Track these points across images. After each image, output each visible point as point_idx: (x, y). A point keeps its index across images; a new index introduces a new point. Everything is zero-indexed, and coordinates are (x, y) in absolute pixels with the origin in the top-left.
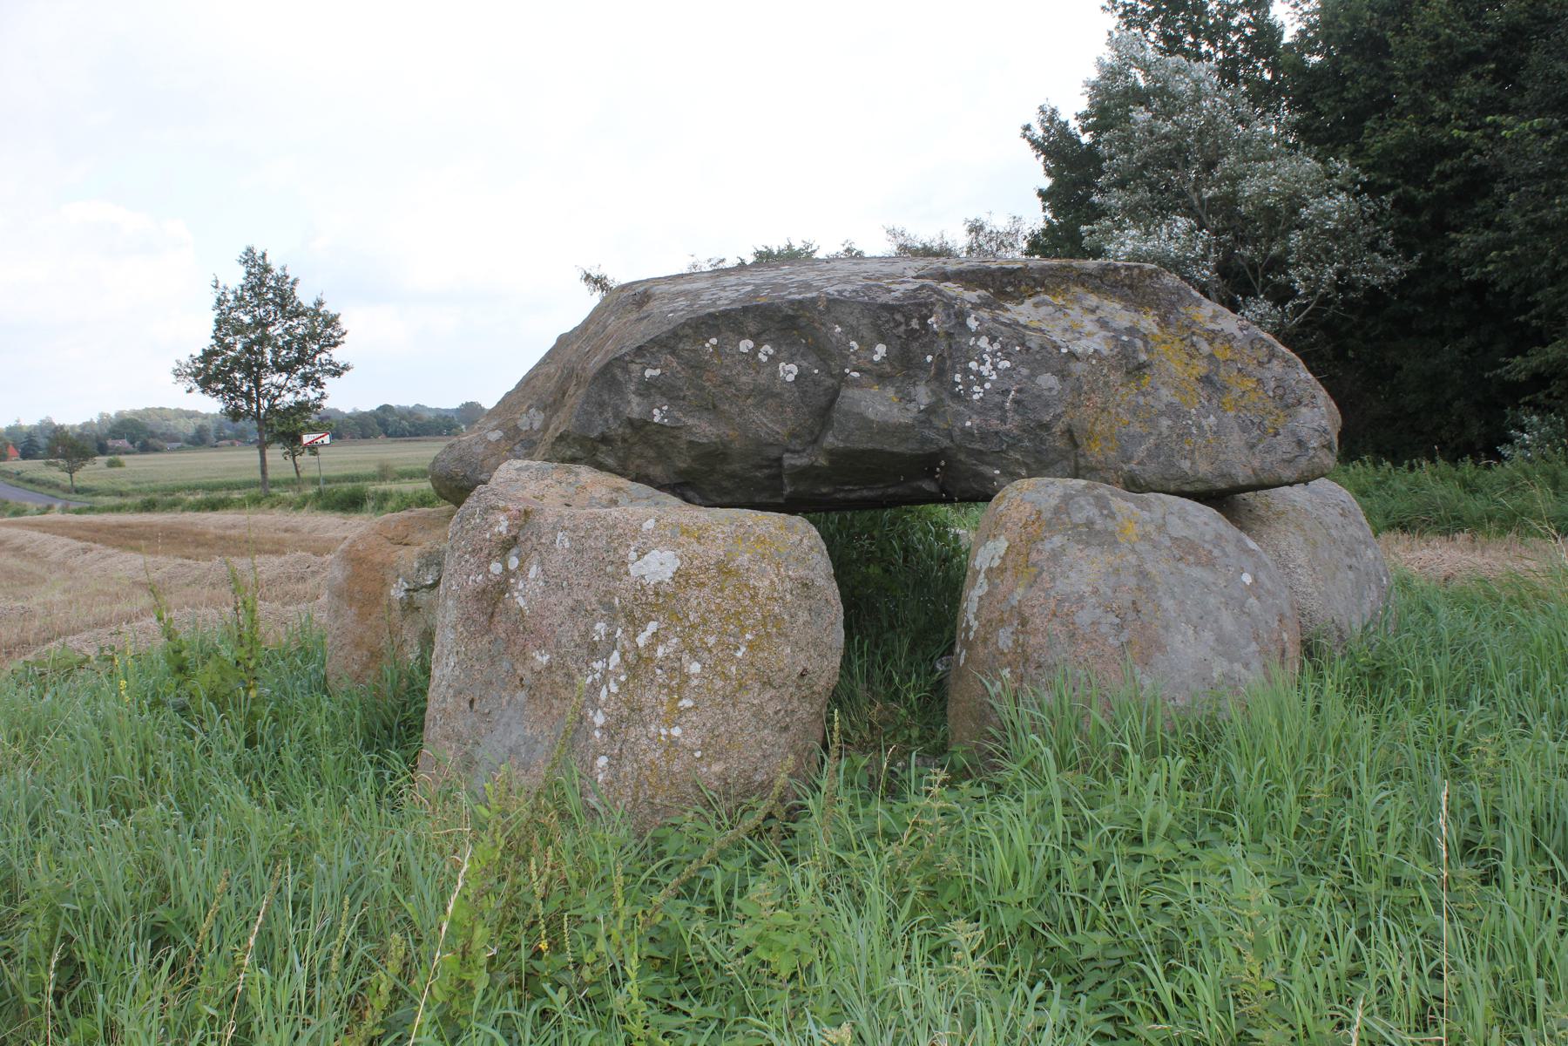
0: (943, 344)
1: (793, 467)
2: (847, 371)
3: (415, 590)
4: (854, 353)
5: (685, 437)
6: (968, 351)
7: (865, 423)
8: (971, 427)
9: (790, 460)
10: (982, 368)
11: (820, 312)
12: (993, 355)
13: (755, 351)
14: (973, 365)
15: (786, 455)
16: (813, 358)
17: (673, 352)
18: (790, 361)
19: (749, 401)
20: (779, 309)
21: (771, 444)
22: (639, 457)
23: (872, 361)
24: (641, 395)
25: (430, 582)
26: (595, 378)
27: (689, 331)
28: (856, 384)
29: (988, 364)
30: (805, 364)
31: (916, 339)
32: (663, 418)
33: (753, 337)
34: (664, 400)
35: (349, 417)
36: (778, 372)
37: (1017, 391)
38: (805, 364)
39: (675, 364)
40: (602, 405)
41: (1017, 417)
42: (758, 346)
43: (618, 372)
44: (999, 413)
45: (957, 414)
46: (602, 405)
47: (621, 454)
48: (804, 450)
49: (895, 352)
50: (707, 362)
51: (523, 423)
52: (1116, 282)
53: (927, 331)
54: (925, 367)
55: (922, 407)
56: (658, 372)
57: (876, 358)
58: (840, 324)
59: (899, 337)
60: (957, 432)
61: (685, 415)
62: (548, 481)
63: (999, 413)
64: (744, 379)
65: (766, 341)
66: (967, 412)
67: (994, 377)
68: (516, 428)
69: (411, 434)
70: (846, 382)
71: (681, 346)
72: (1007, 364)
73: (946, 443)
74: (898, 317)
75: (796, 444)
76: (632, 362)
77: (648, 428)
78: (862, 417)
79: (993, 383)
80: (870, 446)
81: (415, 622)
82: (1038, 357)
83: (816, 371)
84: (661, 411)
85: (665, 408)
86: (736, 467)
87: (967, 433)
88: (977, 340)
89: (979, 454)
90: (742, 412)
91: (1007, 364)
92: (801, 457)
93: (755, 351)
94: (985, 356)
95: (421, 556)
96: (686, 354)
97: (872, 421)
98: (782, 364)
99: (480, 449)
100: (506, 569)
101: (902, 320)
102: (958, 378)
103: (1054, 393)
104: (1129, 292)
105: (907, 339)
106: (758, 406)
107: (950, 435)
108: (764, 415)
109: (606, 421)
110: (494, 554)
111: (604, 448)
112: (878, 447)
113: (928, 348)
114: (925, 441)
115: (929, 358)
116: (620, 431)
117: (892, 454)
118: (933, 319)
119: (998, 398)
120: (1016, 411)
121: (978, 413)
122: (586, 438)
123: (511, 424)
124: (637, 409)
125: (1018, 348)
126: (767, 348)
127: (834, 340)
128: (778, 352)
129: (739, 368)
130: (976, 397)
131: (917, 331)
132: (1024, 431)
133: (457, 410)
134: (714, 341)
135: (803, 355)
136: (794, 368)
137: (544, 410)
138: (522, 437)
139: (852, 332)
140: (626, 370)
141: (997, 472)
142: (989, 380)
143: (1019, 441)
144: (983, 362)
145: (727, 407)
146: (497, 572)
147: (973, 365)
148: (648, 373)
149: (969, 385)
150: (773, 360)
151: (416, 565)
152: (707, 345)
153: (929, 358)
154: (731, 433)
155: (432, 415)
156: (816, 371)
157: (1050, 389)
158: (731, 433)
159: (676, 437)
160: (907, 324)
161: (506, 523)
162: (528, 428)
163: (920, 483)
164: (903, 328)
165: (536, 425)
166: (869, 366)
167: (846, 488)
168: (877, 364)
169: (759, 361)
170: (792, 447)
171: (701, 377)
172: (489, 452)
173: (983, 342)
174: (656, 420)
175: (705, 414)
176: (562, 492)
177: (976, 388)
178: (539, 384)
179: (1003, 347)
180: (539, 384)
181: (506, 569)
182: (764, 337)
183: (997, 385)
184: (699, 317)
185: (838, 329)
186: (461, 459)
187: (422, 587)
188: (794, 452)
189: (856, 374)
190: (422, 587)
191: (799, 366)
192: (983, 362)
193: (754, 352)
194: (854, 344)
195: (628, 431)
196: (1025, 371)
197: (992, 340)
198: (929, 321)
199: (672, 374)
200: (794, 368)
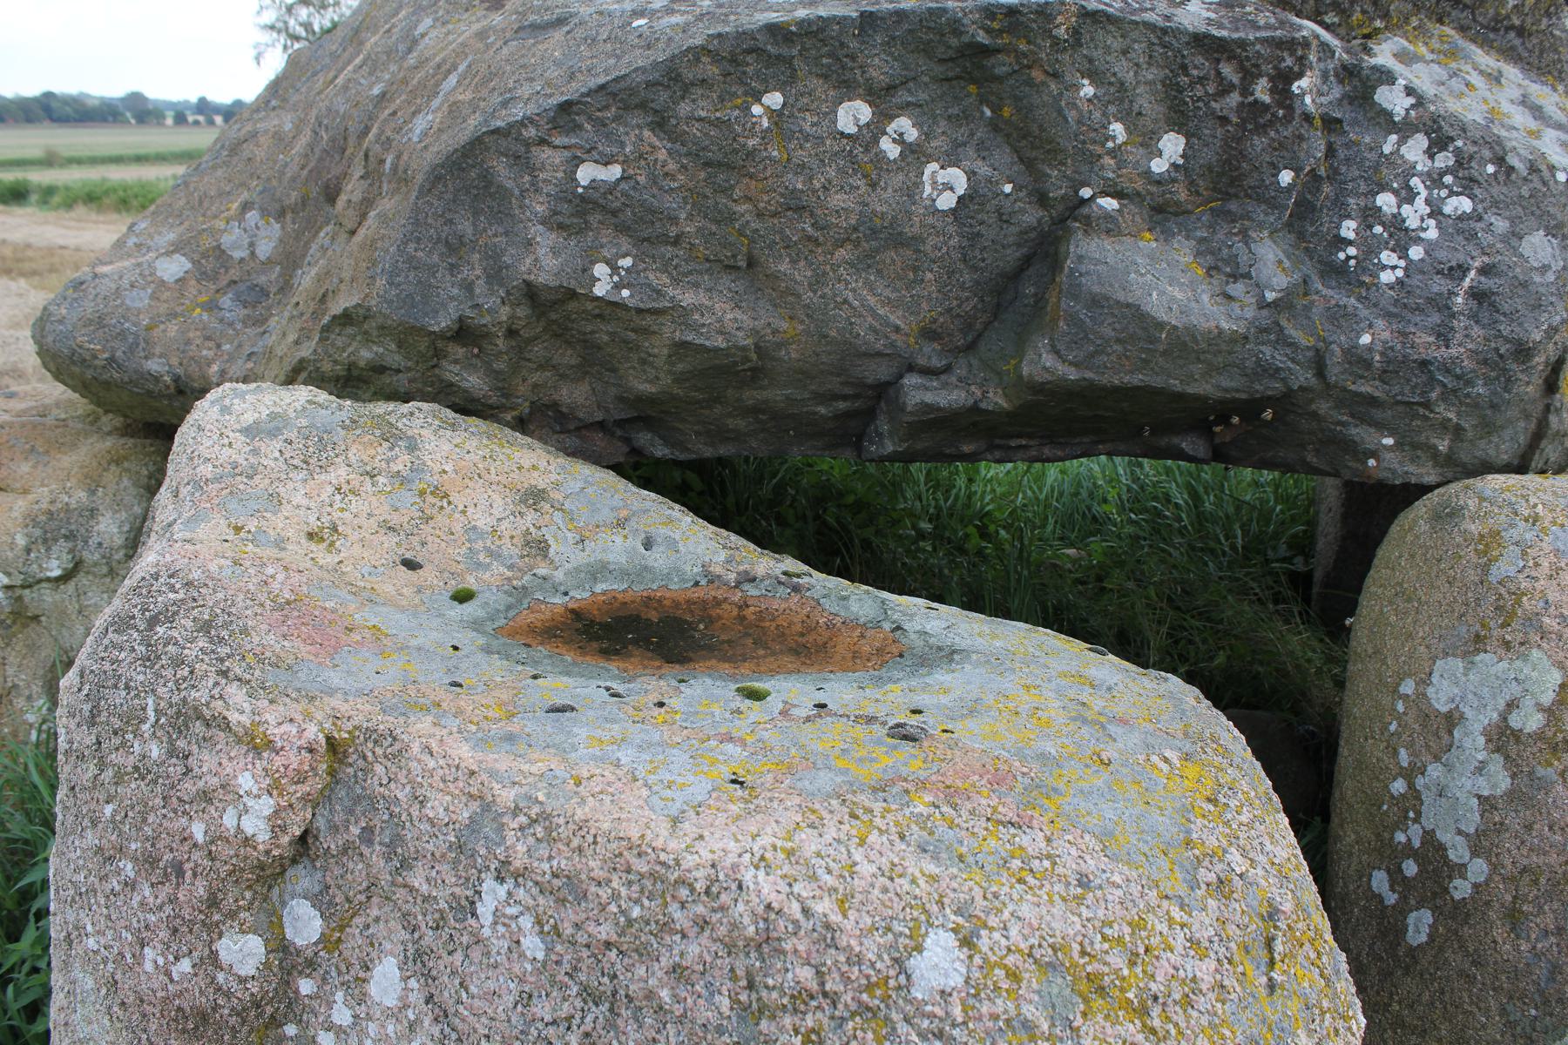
0: (1317, 144)
1: (928, 408)
2: (1086, 193)
3: (26, 586)
4: (1112, 153)
5: (670, 331)
6: (1376, 168)
7: (1139, 323)
8: (1369, 348)
9: (918, 393)
10: (1406, 210)
11: (1056, 41)
12: (1434, 180)
13: (874, 131)
14: (1386, 201)
15: (911, 380)
16: (1003, 156)
17: (660, 124)
18: (950, 160)
19: (841, 253)
20: (956, 27)
21: (879, 354)
22: (541, 367)
23: (1148, 172)
24: (561, 227)
25: (57, 573)
26: (436, 178)
27: (712, 70)
28: (1110, 227)
29: (1420, 202)
30: (983, 170)
31: (1261, 129)
32: (618, 287)
33: (873, 95)
34: (625, 243)
35: (11, 101)
36: (919, 184)
37: (1485, 271)
38: (983, 170)
39: (662, 155)
40: (454, 248)
41: (1477, 331)
42: (883, 116)
43: (502, 170)
44: (1436, 318)
45: (1338, 316)
46: (454, 248)
47: (500, 365)
48: (947, 369)
49: (1208, 155)
50: (751, 154)
51: (233, 239)
52: (1497, 19)
53: (1290, 109)
54: (1269, 197)
55: (1270, 296)
56: (615, 171)
57: (1159, 166)
58: (1094, 76)
59: (1224, 120)
60: (1335, 357)
61: (676, 281)
62: (339, 473)
63: (1436, 318)
64: (837, 200)
65: (905, 108)
66: (1364, 312)
67: (1432, 234)
68: (220, 252)
69: (76, 120)
70: (1087, 222)
71: (684, 108)
72: (1465, 205)
73: (1303, 377)
74: (1227, 70)
75: (930, 354)
76: (542, 142)
77: (572, 306)
78: (1137, 314)
79: (1430, 248)
80: (1137, 379)
81: (33, 648)
82: (1525, 192)
83: (1008, 188)
84: (615, 269)
85: (627, 262)
86: (775, 395)
87: (1358, 360)
88: (1402, 141)
89: (1363, 407)
90: (818, 281)
91: (1465, 205)
92: (945, 385)
93: (874, 131)
94: (1415, 182)
95: (31, 520)
96: (695, 130)
97: (1160, 325)
98: (933, 166)
99: (139, 300)
100: (280, 946)
101: (1236, 79)
102: (1349, 229)
103: (1551, 277)
104: (1517, 42)
105: (1242, 126)
106: (865, 263)
107: (1319, 364)
108: (872, 290)
109: (469, 287)
110: (229, 902)
111: (460, 352)
112: (1158, 382)
113: (1286, 153)
114: (1267, 370)
115: (1286, 177)
116: (504, 313)
117: (1181, 396)
118: (1304, 83)
119: (1439, 285)
120: (1474, 317)
121: (1388, 315)
122: (421, 331)
123: (207, 242)
124: (550, 263)
125: (1490, 169)
126: (905, 125)
127: (1072, 115)
128: (928, 135)
129: (832, 172)
130: (1386, 277)
131: (1266, 107)
132: (1485, 362)
133: (122, 100)
134: (775, 99)
135: (981, 147)
136: (958, 178)
137: (280, 215)
138: (234, 274)
139: (1118, 97)
140: (521, 161)
141: (1389, 441)
142: (1418, 240)
143: (1469, 383)
144: (1409, 196)
145: (784, 267)
146: (248, 969)
147: (1386, 201)
148: (586, 174)
149: (1370, 249)
150: (914, 154)
151: (21, 541)
152: (757, 110)
153: (1286, 177)
154: (785, 325)
155: (97, 103)
156: (1008, 188)
157: (1544, 269)
158: (785, 325)
159: (646, 332)
160: (1246, 91)
161: (266, 805)
162: (244, 254)
163: (1175, 440)
164: (1234, 98)
165: (265, 249)
166: (1139, 185)
167: (1013, 443)
168: (1159, 181)
169: (881, 157)
170: (921, 361)
171: (726, 191)
172: (163, 308)
173: (1415, 150)
174: (600, 290)
175: (726, 280)
176: (384, 512)
177: (1387, 257)
178: (260, 154)
179: (1461, 161)
180: (260, 154)
181: (280, 946)
182: (903, 96)
183: (1441, 255)
184: (742, 35)
185: (1088, 90)
186: (99, 322)
187: (40, 581)
188: (928, 372)
189: (1110, 204)
190: (40, 581)
191: (971, 175)
192: (1409, 196)
193: (900, 140)
194: (1117, 128)
195: (522, 312)
196: (1501, 225)
197: (1439, 143)
198: (1295, 88)
199: (653, 180)
200: (958, 178)
